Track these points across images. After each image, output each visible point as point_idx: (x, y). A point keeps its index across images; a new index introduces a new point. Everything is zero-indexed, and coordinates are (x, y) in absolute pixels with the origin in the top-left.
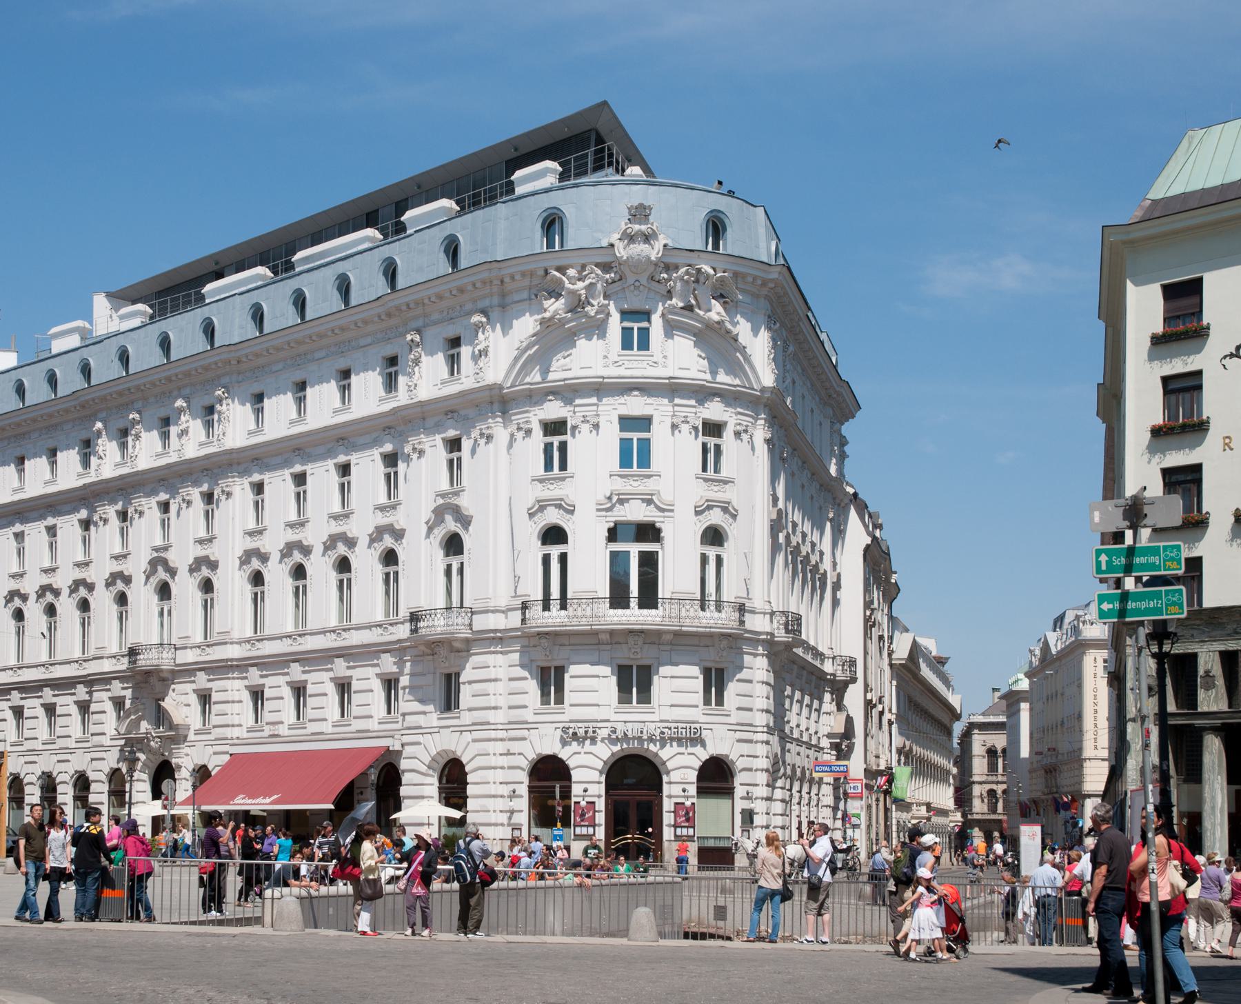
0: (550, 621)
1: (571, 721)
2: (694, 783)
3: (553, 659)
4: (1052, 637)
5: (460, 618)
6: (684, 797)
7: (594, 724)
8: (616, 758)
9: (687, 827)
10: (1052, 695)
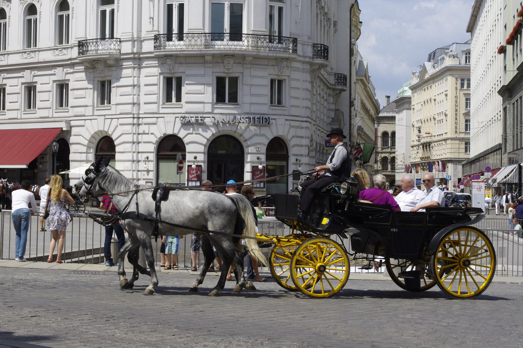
0: (174, 47)
1: (186, 113)
2: (188, 153)
3: (174, 73)
4: (429, 65)
5: (112, 45)
6: (258, 163)
7: (202, 115)
8: (215, 137)
9: (196, 181)
10: (427, 101)
